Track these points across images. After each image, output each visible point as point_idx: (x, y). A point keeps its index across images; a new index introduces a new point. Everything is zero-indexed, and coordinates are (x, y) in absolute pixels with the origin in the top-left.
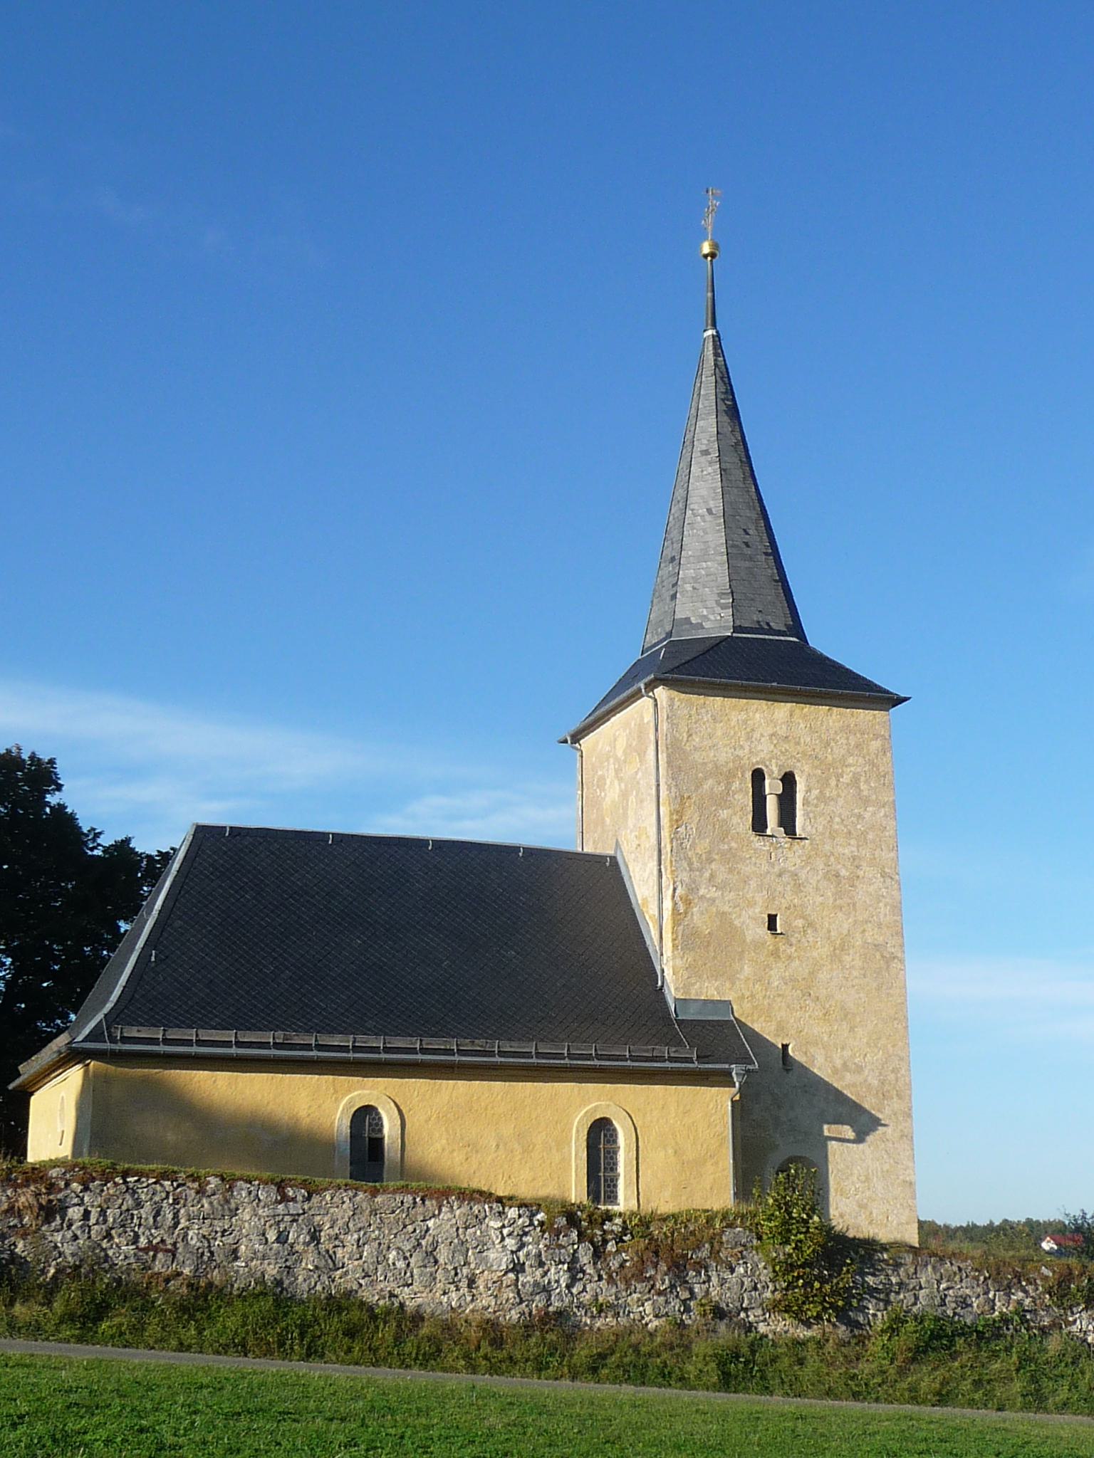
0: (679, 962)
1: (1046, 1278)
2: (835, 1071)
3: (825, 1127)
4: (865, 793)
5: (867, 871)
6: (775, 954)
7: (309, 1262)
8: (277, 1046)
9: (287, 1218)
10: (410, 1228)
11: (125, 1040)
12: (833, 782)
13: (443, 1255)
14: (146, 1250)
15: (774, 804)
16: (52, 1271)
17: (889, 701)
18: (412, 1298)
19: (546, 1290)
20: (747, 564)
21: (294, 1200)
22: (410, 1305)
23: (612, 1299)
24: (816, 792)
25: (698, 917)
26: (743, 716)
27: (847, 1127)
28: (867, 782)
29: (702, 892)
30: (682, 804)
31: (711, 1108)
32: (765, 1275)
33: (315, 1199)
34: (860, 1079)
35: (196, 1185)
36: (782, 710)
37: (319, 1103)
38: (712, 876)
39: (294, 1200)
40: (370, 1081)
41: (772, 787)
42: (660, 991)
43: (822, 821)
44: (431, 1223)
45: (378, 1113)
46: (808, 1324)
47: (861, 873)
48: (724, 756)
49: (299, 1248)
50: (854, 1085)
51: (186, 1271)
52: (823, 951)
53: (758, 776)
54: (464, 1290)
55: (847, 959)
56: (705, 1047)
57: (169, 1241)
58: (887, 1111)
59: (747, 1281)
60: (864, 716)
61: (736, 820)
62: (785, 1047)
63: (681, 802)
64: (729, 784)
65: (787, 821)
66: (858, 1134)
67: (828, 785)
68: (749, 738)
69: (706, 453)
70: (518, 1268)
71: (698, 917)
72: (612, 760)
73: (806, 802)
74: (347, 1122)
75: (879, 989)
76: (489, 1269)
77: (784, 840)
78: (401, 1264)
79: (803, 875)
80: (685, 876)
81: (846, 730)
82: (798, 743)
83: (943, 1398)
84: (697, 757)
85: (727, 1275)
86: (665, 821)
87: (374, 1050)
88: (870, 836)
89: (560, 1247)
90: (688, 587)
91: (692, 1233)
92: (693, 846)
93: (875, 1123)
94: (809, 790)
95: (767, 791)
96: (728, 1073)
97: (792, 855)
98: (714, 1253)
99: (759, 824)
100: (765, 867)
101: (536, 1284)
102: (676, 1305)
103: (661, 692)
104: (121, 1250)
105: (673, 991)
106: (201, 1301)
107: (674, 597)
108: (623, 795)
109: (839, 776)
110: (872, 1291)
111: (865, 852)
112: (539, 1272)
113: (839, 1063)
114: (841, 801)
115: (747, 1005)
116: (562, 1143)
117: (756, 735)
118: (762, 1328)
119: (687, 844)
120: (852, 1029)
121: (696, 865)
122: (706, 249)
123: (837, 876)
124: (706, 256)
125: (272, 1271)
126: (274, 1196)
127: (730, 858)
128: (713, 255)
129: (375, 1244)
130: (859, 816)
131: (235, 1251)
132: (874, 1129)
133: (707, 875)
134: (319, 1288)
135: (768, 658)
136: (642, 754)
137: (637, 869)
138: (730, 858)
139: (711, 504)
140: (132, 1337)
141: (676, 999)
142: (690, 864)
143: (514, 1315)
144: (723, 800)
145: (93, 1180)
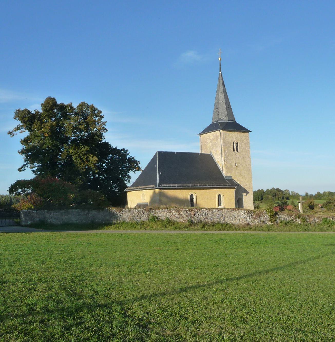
0: (226, 171)
1: (294, 215)
3: (243, 193)
6: (237, 169)
8: (182, 186)
11: (163, 186)
12: (242, 144)
13: (236, 217)
15: (235, 147)
20: (229, 110)
22: (233, 223)
24: (240, 145)
25: (228, 165)
26: (232, 134)
28: (246, 144)
29: (228, 161)
30: (225, 148)
31: (232, 192)
33: (222, 210)
36: (236, 133)
38: (229, 158)
39: (219, 211)
40: (192, 190)
42: (222, 175)
44: (235, 213)
48: (230, 140)
49: (221, 217)
51: (210, 221)
53: (234, 143)
56: (228, 183)
60: (246, 134)
63: (225, 148)
64: (230, 145)
65: (237, 150)
66: (155, 186)
67: (242, 144)
69: (221, 92)
71: (228, 165)
75: (248, 174)
77: (237, 153)
78: (232, 218)
83: (289, 231)
85: (264, 217)
86: (223, 150)
92: (227, 154)
93: (248, 192)
94: (240, 145)
96: (235, 187)
97: (238, 155)
99: (234, 150)
100: (235, 157)
103: (221, 131)
104: (202, 219)
106: (214, 225)
108: (214, 146)
109: (243, 143)
110: (278, 218)
118: (267, 223)
119: (226, 154)
120: (246, 180)
121: (227, 157)
122: (220, 59)
125: (218, 220)
128: (220, 60)
133: (228, 158)
135: (232, 126)
136: (217, 140)
137: (216, 157)
140: (209, 229)
141: (225, 176)
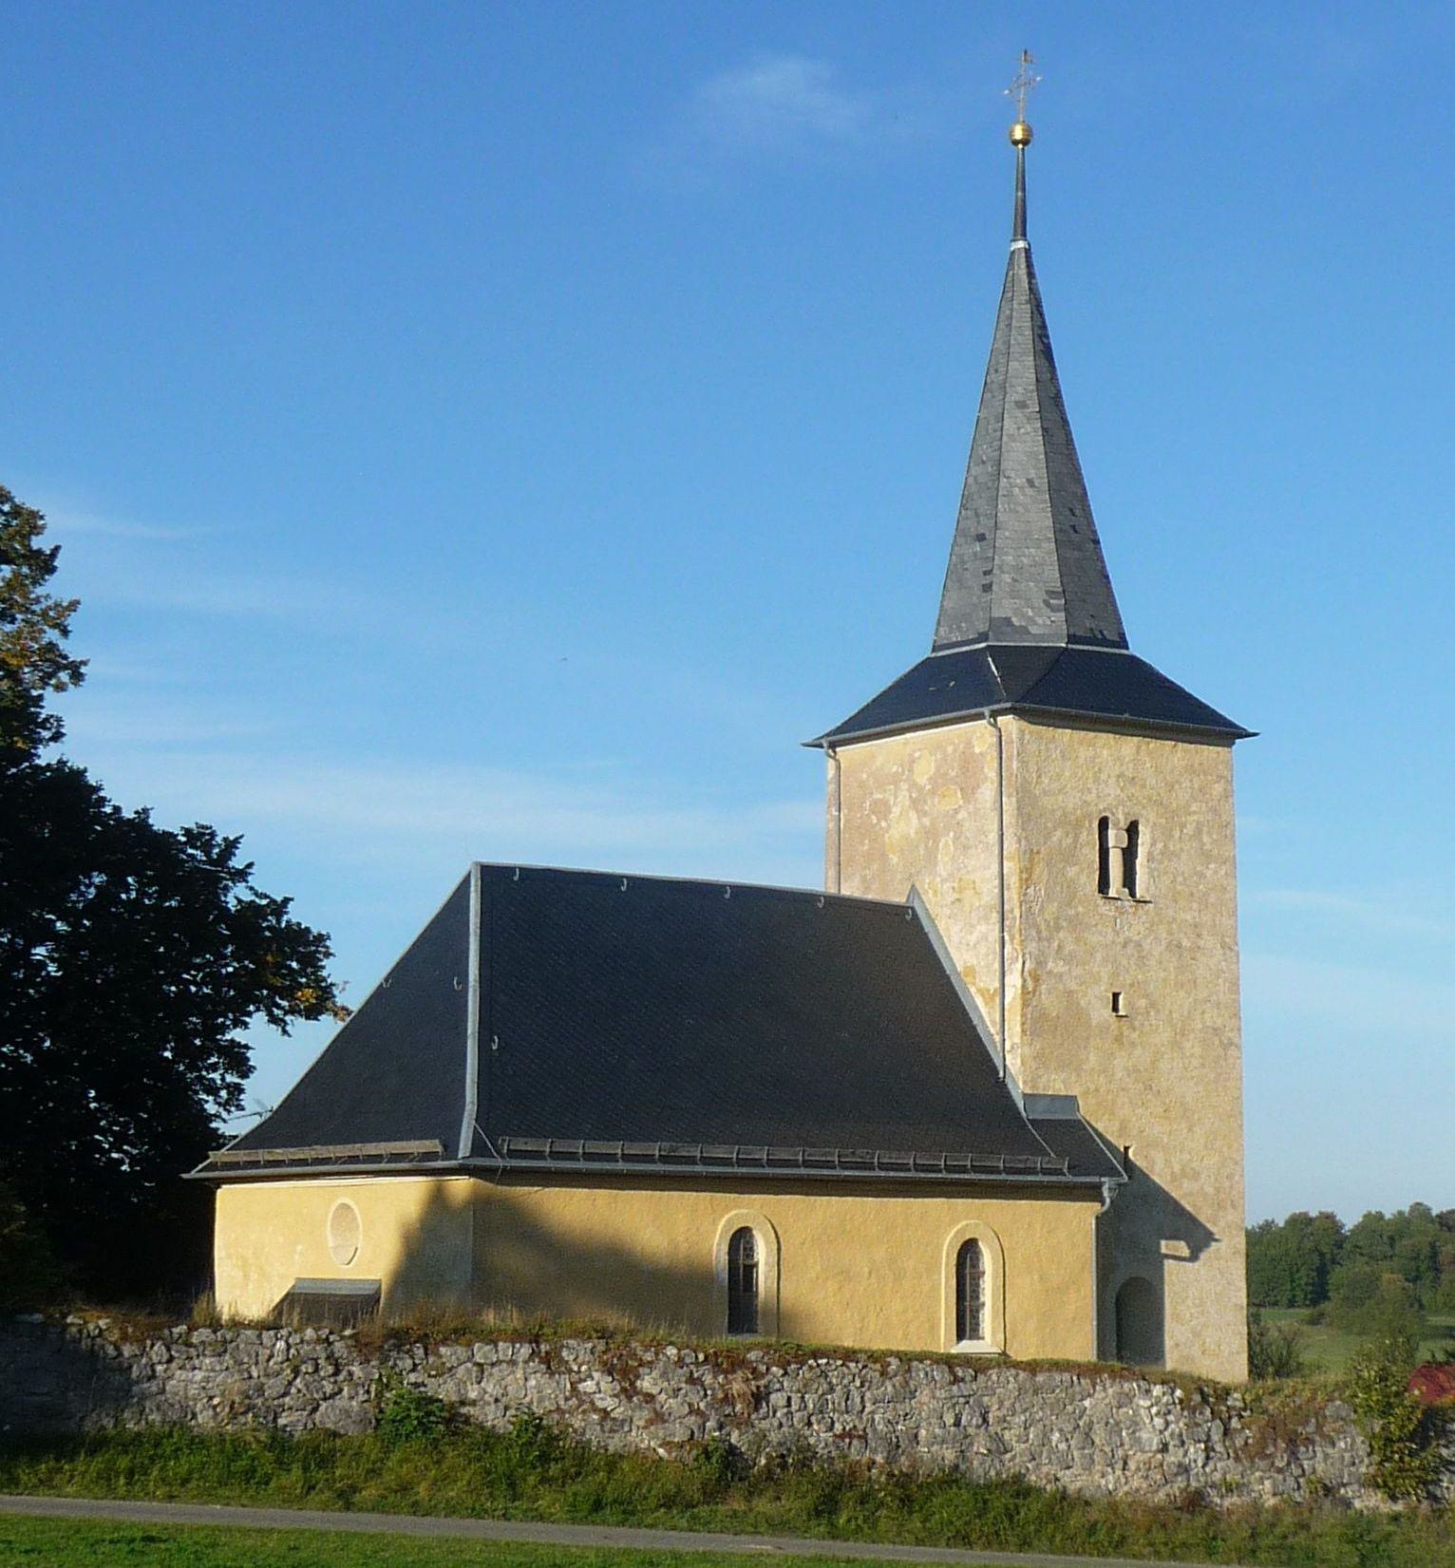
0: (1027, 1050)
2: (1174, 1178)
3: (1163, 1243)
4: (1207, 847)
5: (1208, 941)
6: (1119, 1039)
7: (980, 1446)
8: (664, 1159)
9: (962, 1400)
10: (1070, 1408)
12: (1177, 834)
13: (1099, 1436)
14: (842, 1437)
15: (1117, 856)
16: (763, 1462)
17: (1219, 731)
18: (1073, 1481)
19: (1184, 1469)
21: (963, 1380)
22: (1072, 1488)
23: (1238, 1477)
24: (1160, 846)
26: (1091, 752)
27: (1183, 1243)
29: (1050, 965)
30: (1031, 860)
32: (1362, 1449)
33: (981, 1378)
34: (1196, 1186)
35: (878, 1366)
36: (1129, 746)
37: (674, 1225)
41: (1116, 838)
42: (1003, 1085)
43: (1166, 880)
44: (1087, 1403)
45: (752, 1236)
46: (1394, 1498)
47: (1202, 943)
48: (1072, 801)
49: (971, 1431)
50: (1191, 1194)
51: (879, 1459)
52: (1165, 1036)
53: (1104, 824)
54: (1119, 1472)
55: (1188, 1045)
56: (1043, 1152)
57: (860, 1427)
58: (1222, 1224)
59: (1347, 1456)
60: (1209, 753)
61: (1083, 879)
62: (1126, 1149)
63: (1030, 856)
65: (1129, 881)
67: (1171, 836)
68: (1096, 780)
69: (1021, 405)
70: (1164, 1448)
71: (1048, 1000)
72: (904, 786)
73: (1150, 858)
74: (725, 1248)
76: (1143, 1452)
77: (1129, 903)
78: (1063, 1446)
79: (1146, 946)
80: (1032, 947)
81: (1190, 770)
82: (1144, 786)
84: (1047, 802)
85: (1330, 1451)
87: (726, 1162)
88: (1211, 900)
89: (1198, 1425)
90: (1007, 578)
91: (1300, 1407)
93: (1209, 1237)
94: (1153, 844)
95: (1111, 844)
96: (1098, 1187)
97: (1135, 925)
98: (1319, 1427)
100: (1110, 937)
101: (1180, 1465)
102: (1291, 1483)
103: (1007, 721)
104: (819, 1437)
105: (1019, 1085)
107: (987, 588)
108: (948, 841)
109: (1183, 826)
111: (1206, 918)
112: (1181, 1452)
113: (1177, 1168)
114: (1184, 857)
115: (1092, 1101)
116: (933, 1267)
117: (1104, 777)
118: (1357, 1504)
121: (1044, 934)
122: (1018, 134)
123: (1179, 946)
124: (1016, 143)
125: (950, 1455)
126: (948, 1377)
127: (1076, 924)
128: (1025, 142)
129: (1040, 1426)
130: (1201, 875)
131: (916, 1436)
132: (1207, 1245)
134: (993, 1473)
138: (1076, 924)
139: (1032, 474)
141: (1025, 1095)
142: (1039, 932)
143: (1162, 1494)
144: (1070, 856)
145: (789, 1363)
